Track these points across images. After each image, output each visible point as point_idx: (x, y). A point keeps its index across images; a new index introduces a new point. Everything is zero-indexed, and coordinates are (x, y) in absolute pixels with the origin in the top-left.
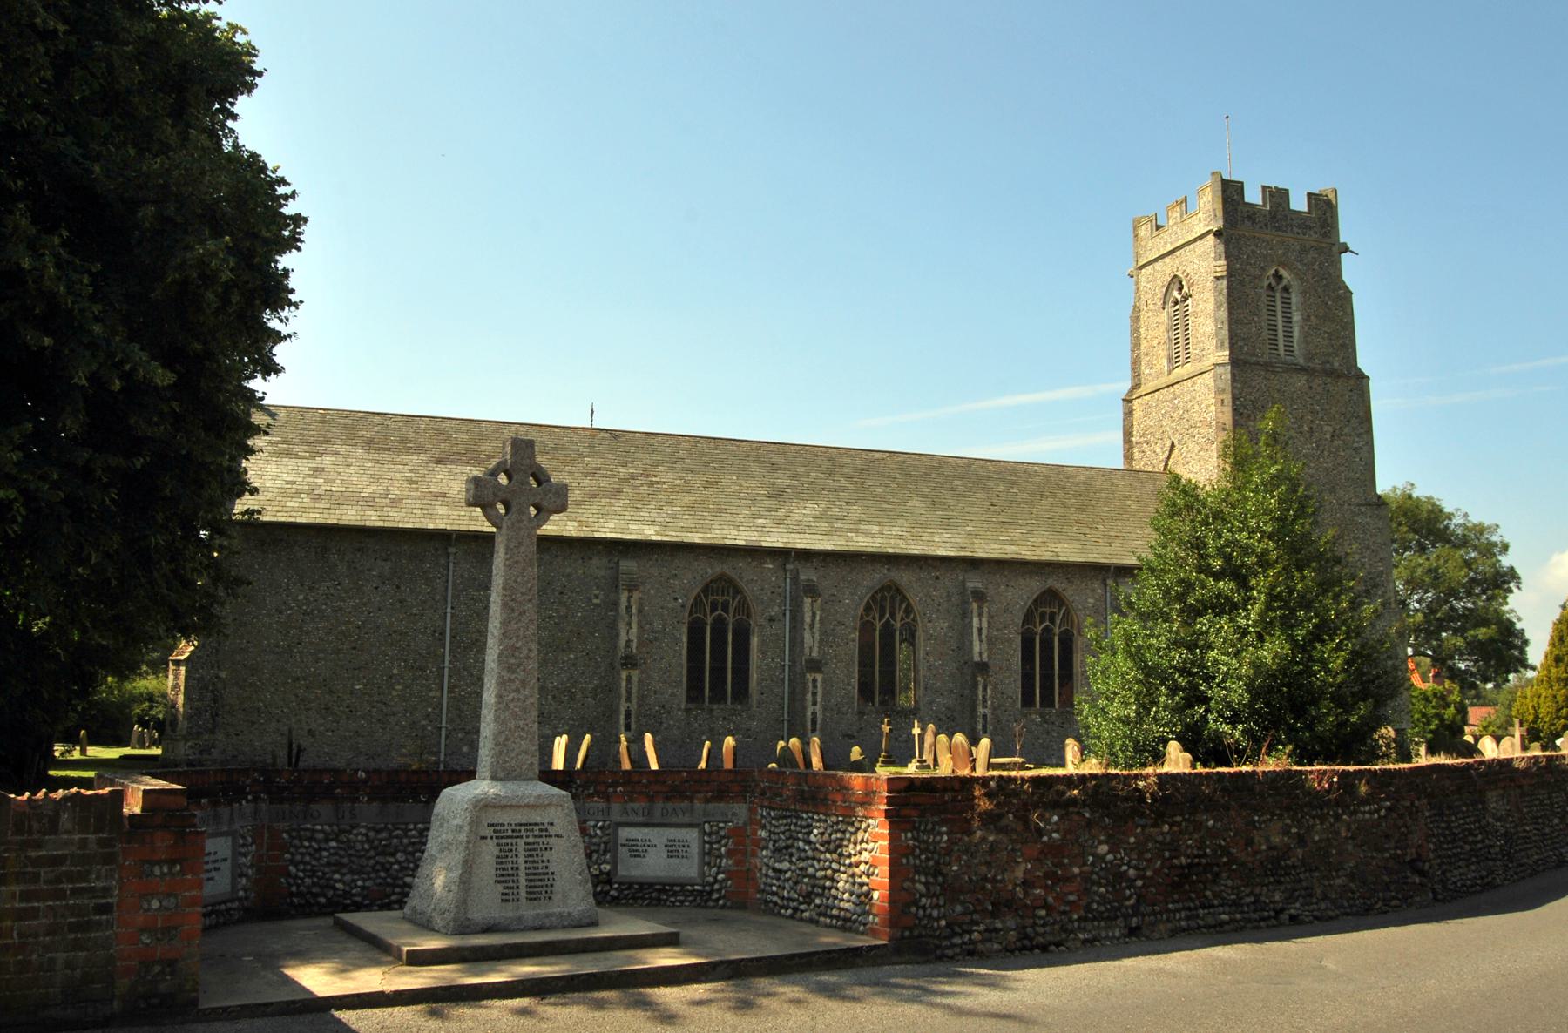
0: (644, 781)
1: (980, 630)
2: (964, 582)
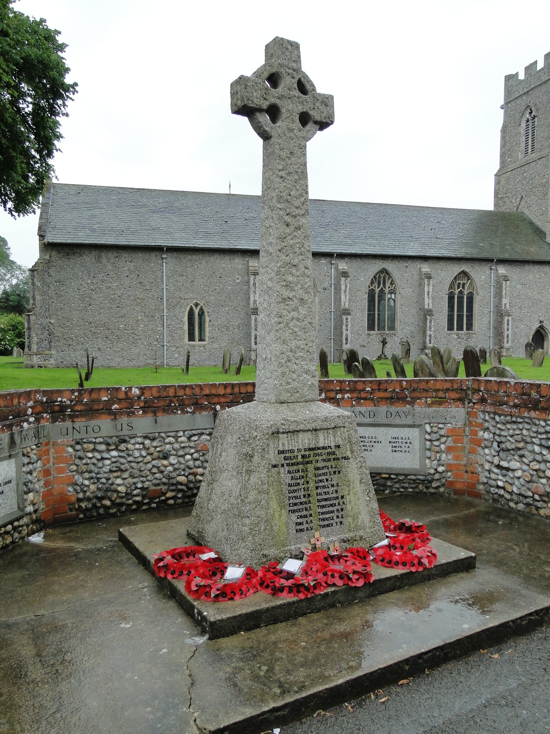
0: (369, 389)
1: (428, 292)
2: (420, 269)
